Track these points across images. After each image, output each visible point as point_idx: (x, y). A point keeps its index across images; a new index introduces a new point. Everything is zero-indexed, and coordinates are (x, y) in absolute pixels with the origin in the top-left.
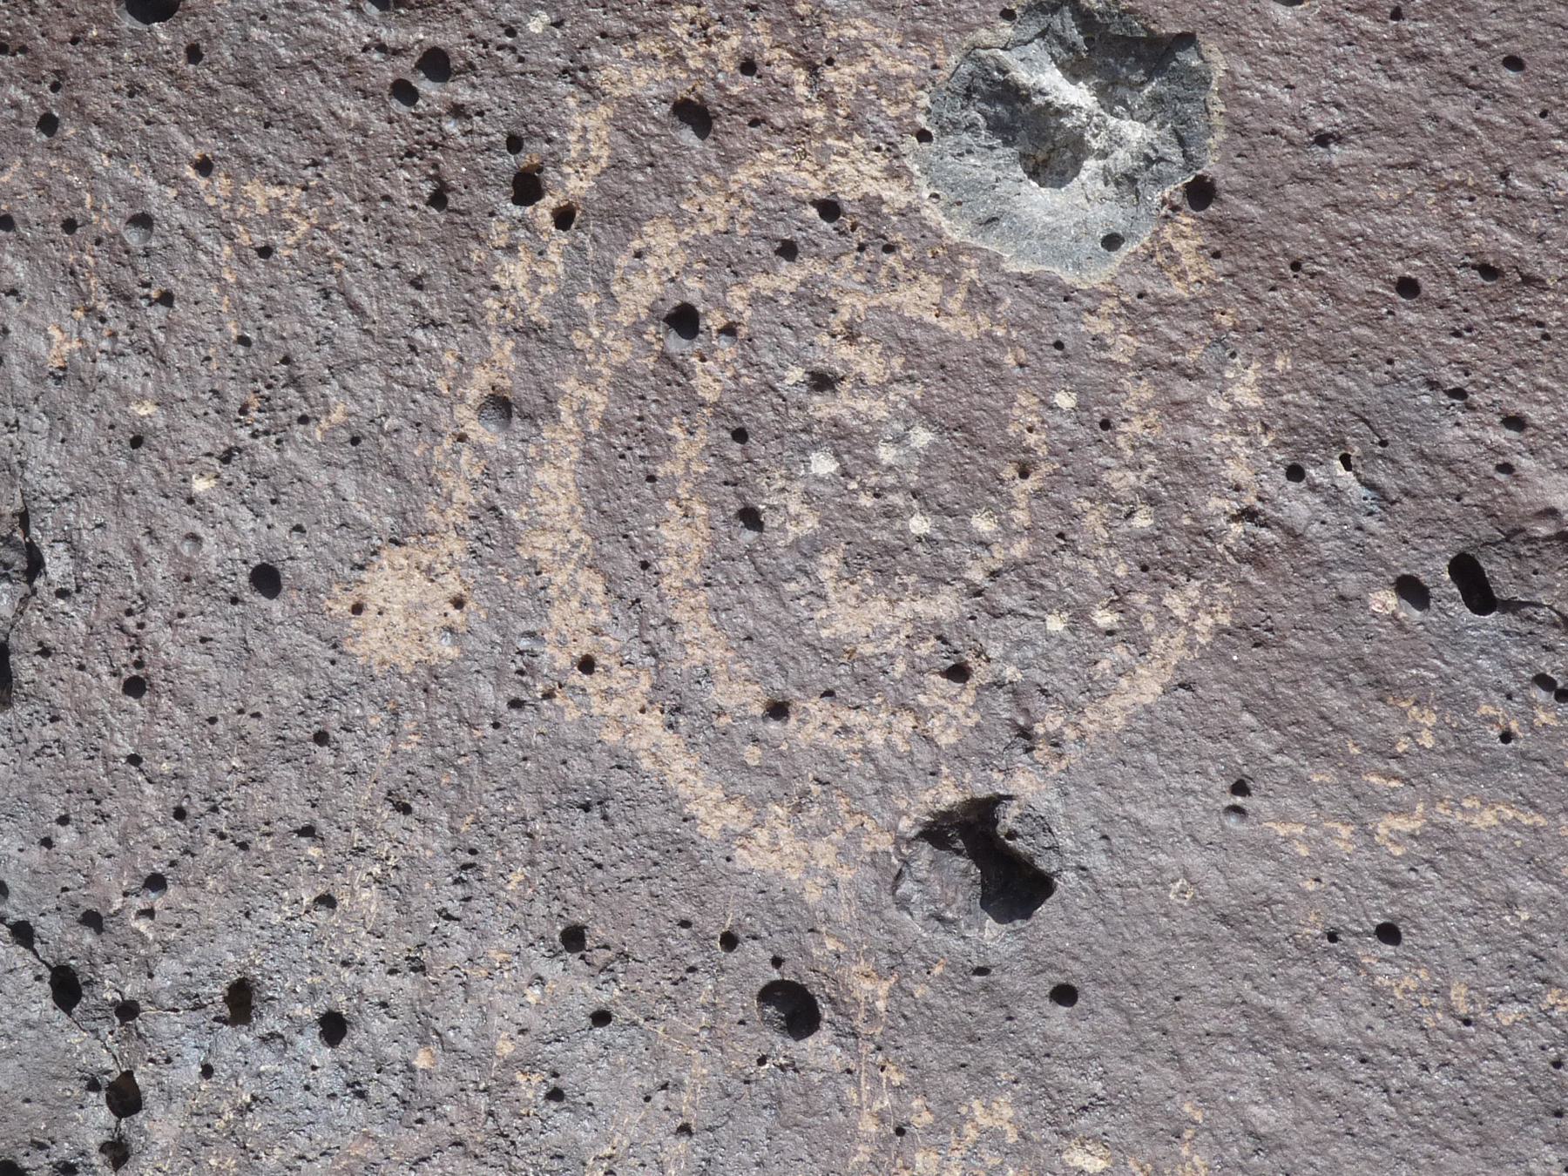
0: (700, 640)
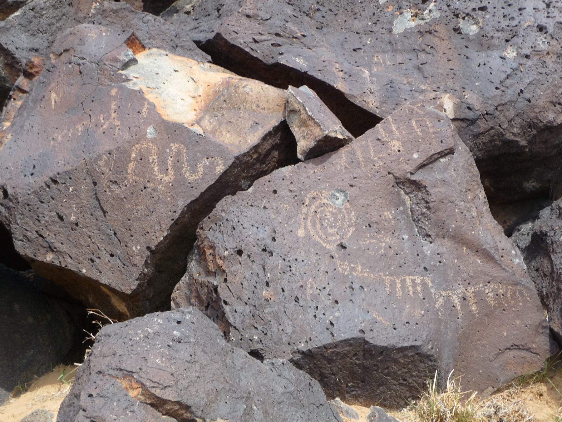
0: (321, 233)
